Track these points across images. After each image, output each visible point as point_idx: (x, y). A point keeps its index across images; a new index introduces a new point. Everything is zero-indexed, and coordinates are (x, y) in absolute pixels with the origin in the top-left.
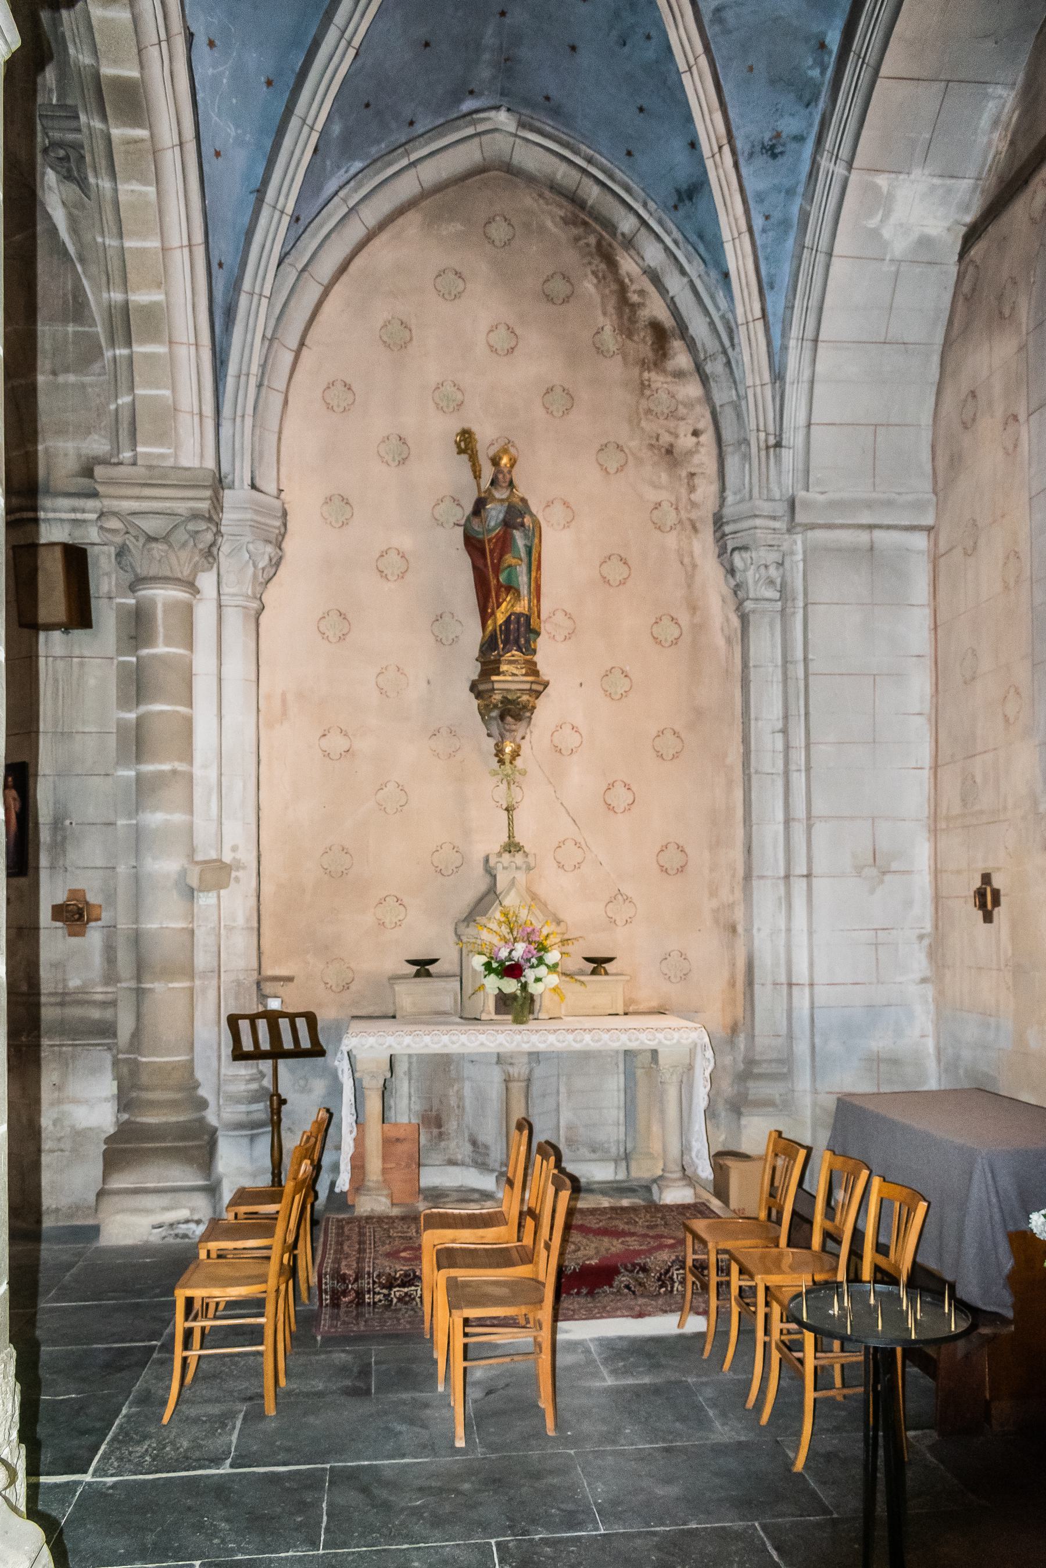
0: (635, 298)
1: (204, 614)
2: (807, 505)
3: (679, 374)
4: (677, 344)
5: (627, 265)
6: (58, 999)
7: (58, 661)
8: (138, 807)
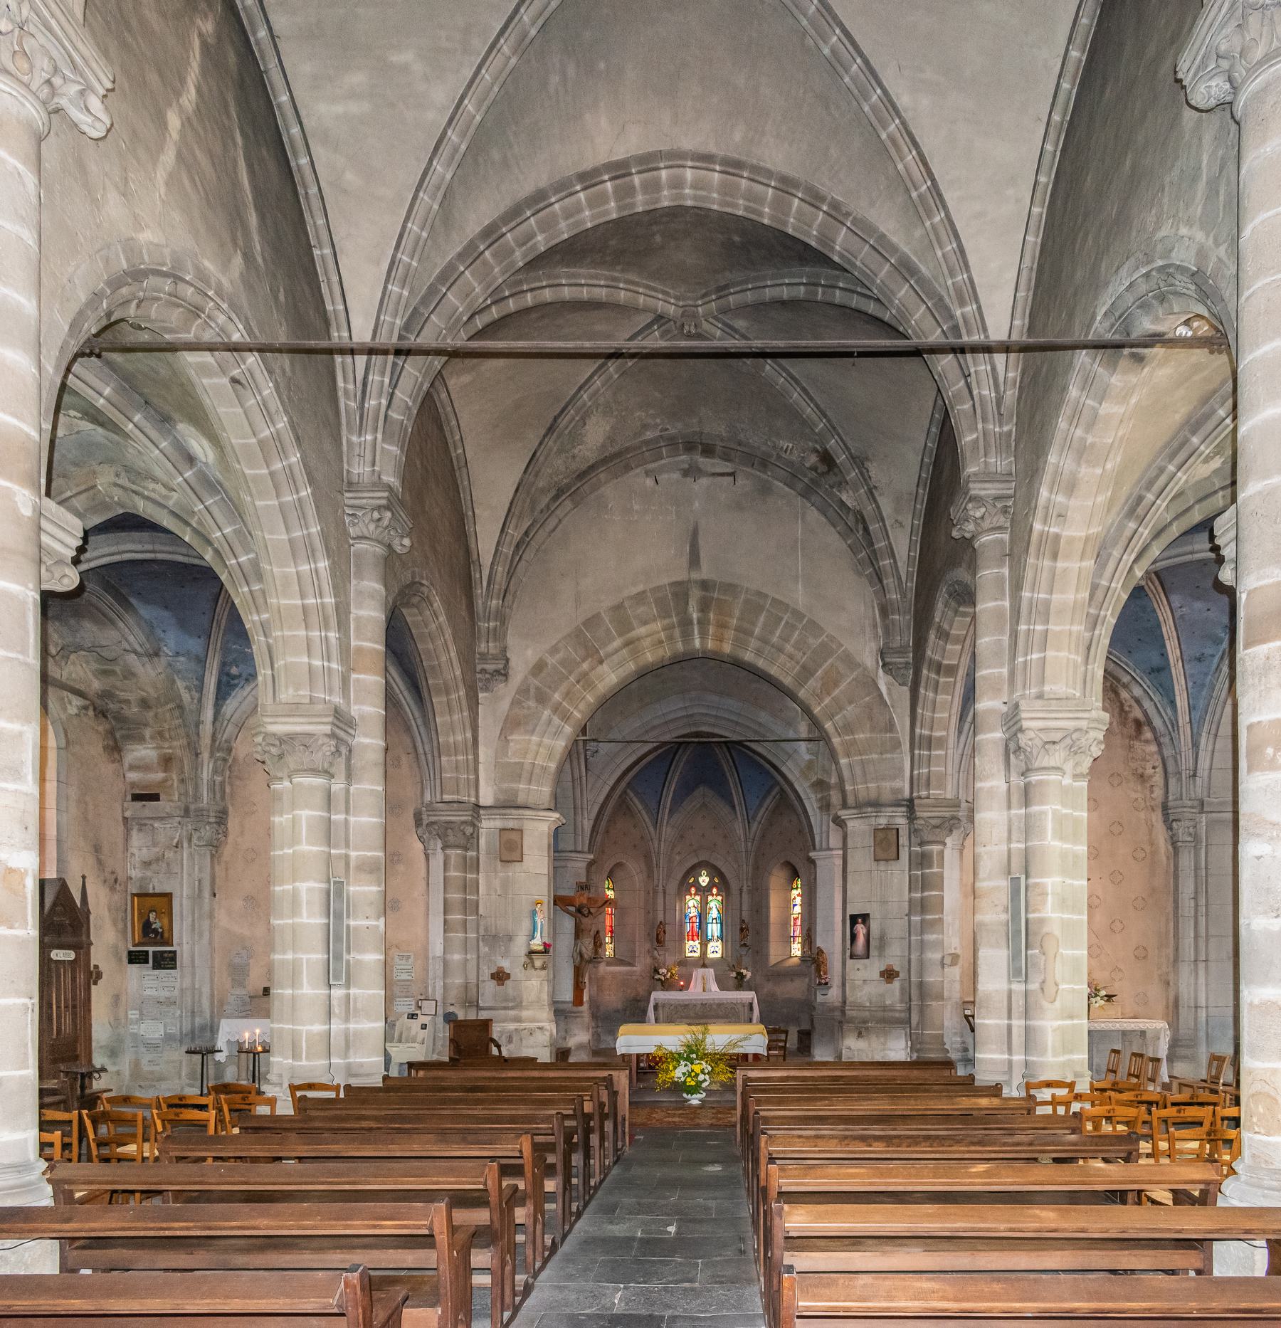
0: (1127, 709)
1: (947, 853)
2: (1210, 804)
3: (1147, 742)
4: (1146, 728)
5: (1124, 694)
8: (922, 933)
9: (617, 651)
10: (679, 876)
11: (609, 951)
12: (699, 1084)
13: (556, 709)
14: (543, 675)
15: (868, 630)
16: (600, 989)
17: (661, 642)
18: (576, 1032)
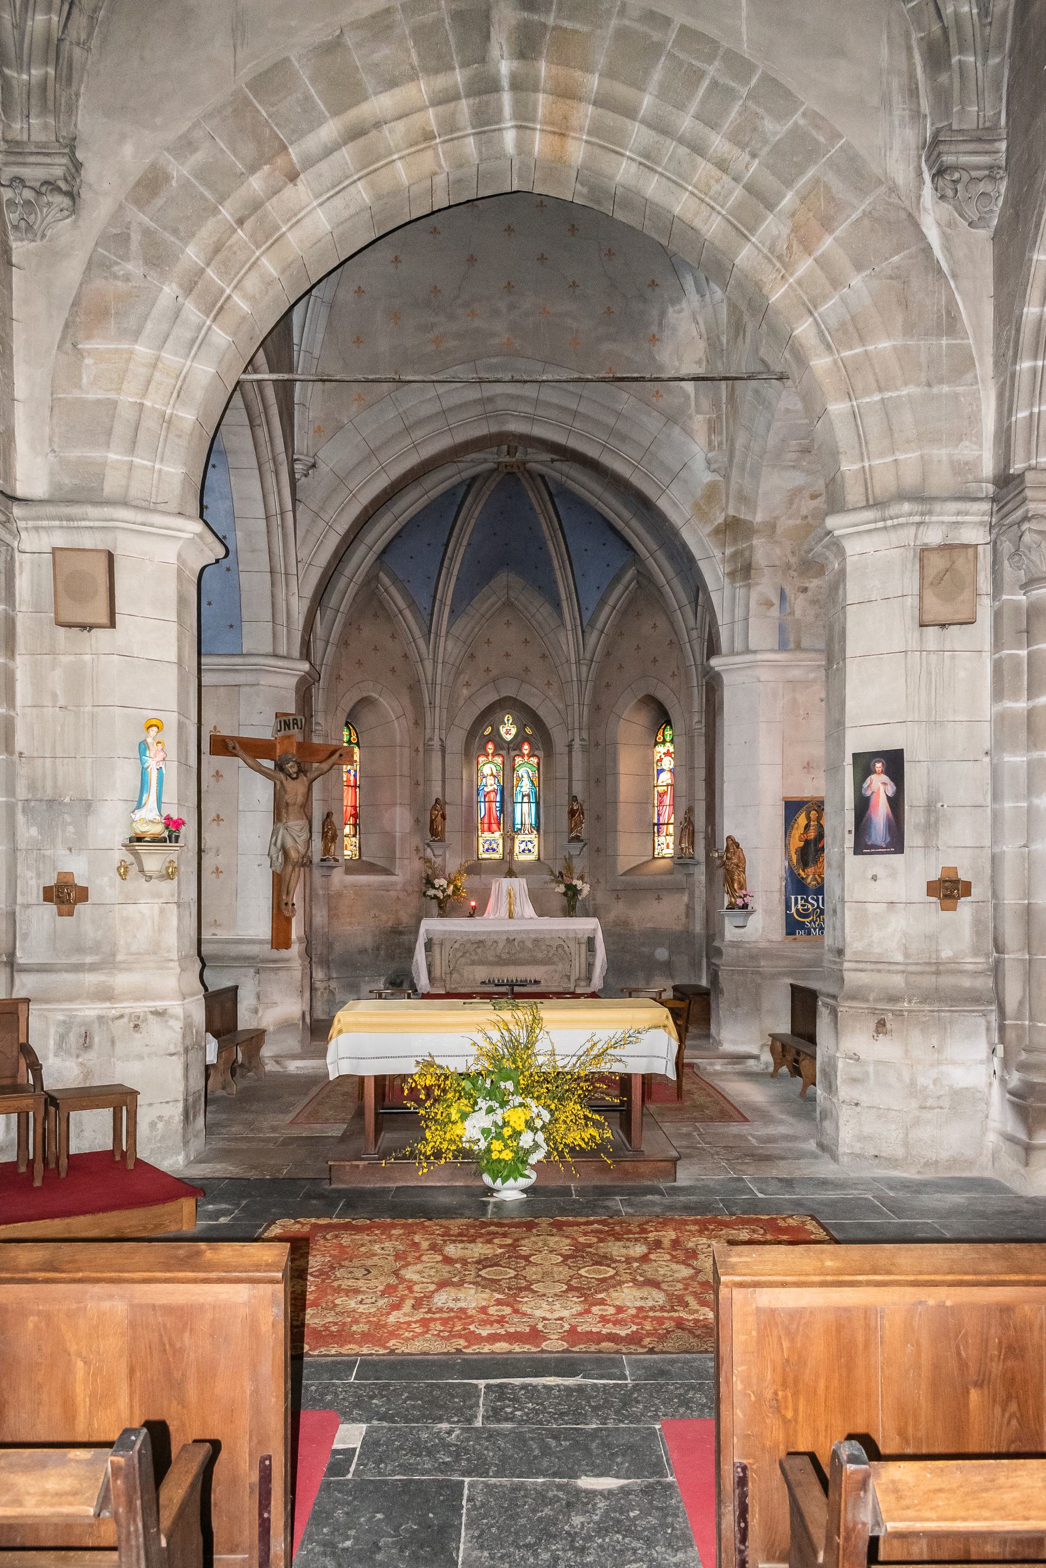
6: (934, 969)
7: (932, 655)
9: (328, 151)
10: (467, 724)
11: (349, 848)
12: (521, 1157)
13: (191, 284)
14: (159, 202)
15: (897, 98)
16: (333, 913)
17: (428, 136)
18: (277, 998)
